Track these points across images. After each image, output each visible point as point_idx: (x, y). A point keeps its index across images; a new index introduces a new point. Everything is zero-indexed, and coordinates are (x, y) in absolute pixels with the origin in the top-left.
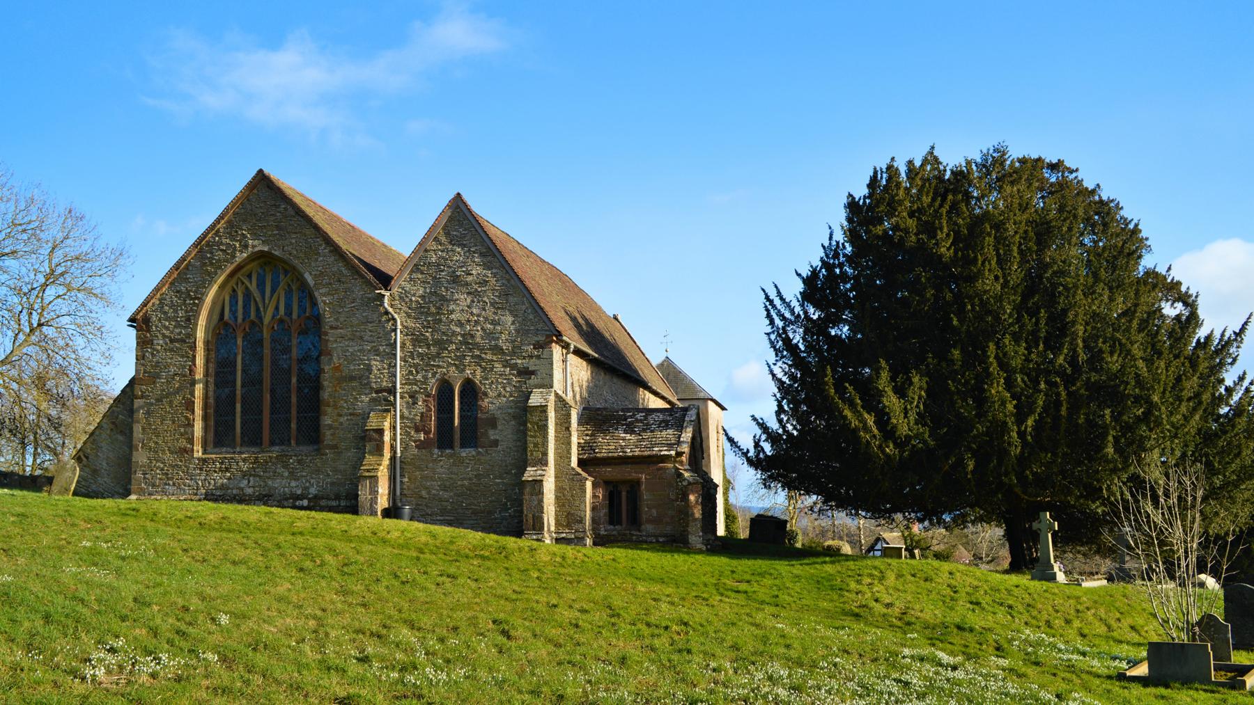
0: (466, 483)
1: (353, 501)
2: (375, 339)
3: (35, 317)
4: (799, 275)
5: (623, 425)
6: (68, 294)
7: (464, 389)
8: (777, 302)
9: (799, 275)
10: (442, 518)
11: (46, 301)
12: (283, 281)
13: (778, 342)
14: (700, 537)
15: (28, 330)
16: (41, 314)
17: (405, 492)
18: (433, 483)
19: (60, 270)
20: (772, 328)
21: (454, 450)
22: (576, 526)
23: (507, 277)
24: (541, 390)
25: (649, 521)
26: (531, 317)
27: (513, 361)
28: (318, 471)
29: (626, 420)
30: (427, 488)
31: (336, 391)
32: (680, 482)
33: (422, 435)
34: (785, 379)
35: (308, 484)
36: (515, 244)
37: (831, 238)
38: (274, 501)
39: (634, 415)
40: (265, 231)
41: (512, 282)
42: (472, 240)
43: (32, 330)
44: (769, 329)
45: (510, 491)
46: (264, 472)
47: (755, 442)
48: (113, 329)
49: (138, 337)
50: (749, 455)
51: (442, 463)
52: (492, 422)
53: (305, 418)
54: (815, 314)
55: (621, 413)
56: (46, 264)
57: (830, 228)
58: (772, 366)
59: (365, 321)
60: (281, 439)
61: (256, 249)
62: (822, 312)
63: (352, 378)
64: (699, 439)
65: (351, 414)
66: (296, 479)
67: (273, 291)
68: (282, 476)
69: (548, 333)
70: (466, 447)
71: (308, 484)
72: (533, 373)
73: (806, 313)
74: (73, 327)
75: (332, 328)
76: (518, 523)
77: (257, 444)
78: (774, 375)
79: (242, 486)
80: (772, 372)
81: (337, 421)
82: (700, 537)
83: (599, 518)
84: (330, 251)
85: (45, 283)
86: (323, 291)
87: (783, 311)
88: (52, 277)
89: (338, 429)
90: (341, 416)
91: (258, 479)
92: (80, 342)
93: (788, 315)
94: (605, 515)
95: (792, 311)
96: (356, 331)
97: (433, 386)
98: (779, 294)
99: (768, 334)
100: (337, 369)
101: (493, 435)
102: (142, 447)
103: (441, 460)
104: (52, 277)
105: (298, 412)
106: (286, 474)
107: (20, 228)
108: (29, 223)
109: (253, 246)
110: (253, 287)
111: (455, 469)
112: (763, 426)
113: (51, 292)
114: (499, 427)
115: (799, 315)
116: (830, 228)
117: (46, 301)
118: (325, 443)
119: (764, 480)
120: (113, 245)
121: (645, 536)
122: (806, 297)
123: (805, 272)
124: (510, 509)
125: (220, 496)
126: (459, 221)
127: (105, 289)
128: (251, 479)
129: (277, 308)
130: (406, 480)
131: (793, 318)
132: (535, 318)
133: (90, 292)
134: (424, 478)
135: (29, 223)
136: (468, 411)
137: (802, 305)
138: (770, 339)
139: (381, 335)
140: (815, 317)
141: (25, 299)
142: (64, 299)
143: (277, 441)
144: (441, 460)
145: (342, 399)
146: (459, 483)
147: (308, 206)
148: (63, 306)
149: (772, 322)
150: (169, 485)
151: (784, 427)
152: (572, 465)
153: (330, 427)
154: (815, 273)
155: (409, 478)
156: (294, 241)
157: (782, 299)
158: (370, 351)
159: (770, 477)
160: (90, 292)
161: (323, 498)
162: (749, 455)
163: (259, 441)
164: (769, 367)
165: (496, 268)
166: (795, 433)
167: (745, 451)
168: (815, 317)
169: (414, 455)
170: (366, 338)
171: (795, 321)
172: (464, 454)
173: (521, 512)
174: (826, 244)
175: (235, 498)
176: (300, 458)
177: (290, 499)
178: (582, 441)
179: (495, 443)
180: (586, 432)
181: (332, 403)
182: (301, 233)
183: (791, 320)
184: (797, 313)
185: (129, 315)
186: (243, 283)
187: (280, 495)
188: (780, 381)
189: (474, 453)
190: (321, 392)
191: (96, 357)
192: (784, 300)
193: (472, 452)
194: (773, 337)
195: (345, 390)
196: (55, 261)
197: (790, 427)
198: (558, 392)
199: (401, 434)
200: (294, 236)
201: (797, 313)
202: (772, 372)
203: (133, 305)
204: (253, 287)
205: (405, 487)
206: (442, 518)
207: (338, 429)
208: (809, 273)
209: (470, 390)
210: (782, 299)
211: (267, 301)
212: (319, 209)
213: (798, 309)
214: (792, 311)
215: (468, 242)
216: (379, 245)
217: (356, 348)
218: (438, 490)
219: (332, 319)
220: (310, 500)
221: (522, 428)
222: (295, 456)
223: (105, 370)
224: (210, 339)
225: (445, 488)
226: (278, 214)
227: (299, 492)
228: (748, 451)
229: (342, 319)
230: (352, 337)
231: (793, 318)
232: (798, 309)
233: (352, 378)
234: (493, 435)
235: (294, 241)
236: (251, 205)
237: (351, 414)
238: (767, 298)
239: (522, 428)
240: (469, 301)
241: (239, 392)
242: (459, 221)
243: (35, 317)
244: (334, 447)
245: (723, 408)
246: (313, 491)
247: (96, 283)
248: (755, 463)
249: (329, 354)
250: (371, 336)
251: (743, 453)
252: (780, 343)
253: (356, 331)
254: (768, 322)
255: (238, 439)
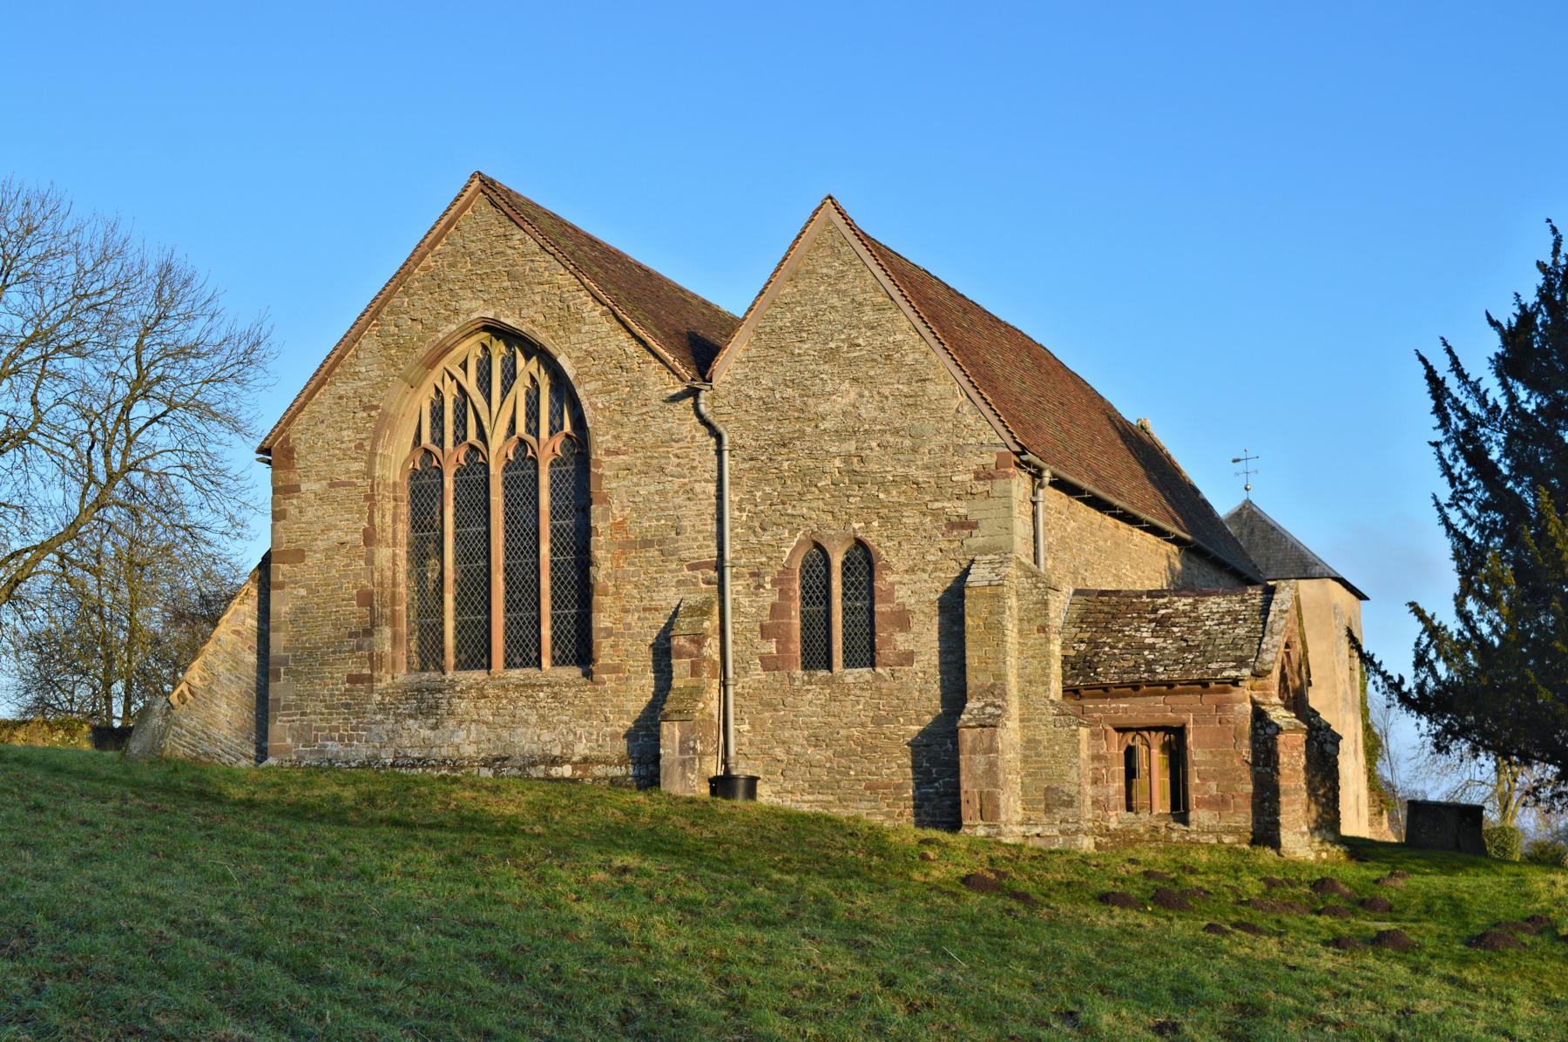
0: (855, 732)
1: (651, 768)
2: (686, 472)
3: (117, 458)
4: (1495, 324)
5: (1151, 621)
6: (170, 414)
7: (848, 559)
8: (1452, 382)
9: (1495, 324)
10: (811, 798)
11: (133, 430)
12: (526, 367)
13: (1456, 460)
14: (1303, 834)
15: (102, 478)
16: (124, 455)
17: (745, 749)
18: (795, 733)
19: (154, 373)
20: (1447, 432)
21: (831, 671)
22: (1061, 813)
23: (924, 347)
24: (991, 557)
25: (1201, 803)
26: (970, 420)
27: (937, 505)
28: (588, 714)
29: (1155, 611)
30: (784, 743)
31: (618, 566)
32: (1262, 727)
33: (774, 645)
34: (1471, 533)
35: (571, 737)
36: (942, 290)
37: (1556, 251)
38: (512, 767)
39: (1171, 602)
40: (487, 282)
41: (933, 356)
42: (857, 282)
43: (111, 477)
44: (1439, 436)
45: (936, 748)
46: (493, 715)
47: (1417, 654)
48: (245, 475)
49: (274, 481)
50: (1405, 688)
51: (810, 696)
52: (902, 620)
53: (566, 617)
54: (1530, 401)
55: (1145, 599)
56: (132, 363)
57: (1554, 230)
58: (1446, 510)
59: (667, 437)
60: (524, 652)
61: (475, 316)
62: (1546, 396)
63: (646, 544)
64: (1299, 647)
65: (645, 609)
66: (552, 727)
67: (506, 389)
68: (526, 722)
69: (1001, 449)
70: (854, 666)
71: (571, 737)
72: (973, 526)
73: (1512, 398)
74: (179, 471)
75: (608, 452)
76: (951, 806)
77: (482, 667)
78: (1450, 527)
79: (457, 740)
80: (1445, 520)
81: (620, 620)
82: (1303, 834)
83: (1107, 799)
84: (603, 314)
85: (131, 395)
86: (591, 386)
87: (1463, 399)
88: (141, 388)
89: (623, 635)
90: (627, 611)
91: (485, 728)
92: (188, 493)
93: (1473, 408)
94: (1118, 792)
95: (1483, 401)
96: (652, 457)
97: (791, 549)
98: (1455, 362)
99: (1437, 444)
100: (619, 526)
101: (902, 641)
102: (285, 674)
103: (808, 691)
104: (141, 388)
105: (553, 608)
106: (534, 719)
107: (86, 302)
108: (101, 293)
109: (469, 312)
110: (471, 385)
111: (835, 707)
112: (1434, 630)
113: (141, 411)
114: (915, 629)
115: (1496, 407)
116: (1554, 230)
117: (133, 430)
118: (600, 661)
119: (1436, 736)
120: (242, 327)
121: (1198, 833)
122: (1506, 367)
123: (1507, 315)
124: (936, 780)
125: (419, 760)
126: (832, 247)
127: (232, 405)
128: (473, 727)
129: (513, 421)
130: (746, 727)
131: (1483, 415)
132: (977, 421)
133: (205, 411)
134: (782, 724)
135: (101, 293)
136: (856, 599)
137: (1504, 384)
138: (1441, 457)
139: (695, 464)
140: (1531, 407)
141: (97, 424)
142: (163, 423)
143: (518, 660)
144: (808, 691)
145: (630, 582)
146: (842, 732)
147: (563, 235)
148: (162, 437)
149: (1445, 421)
150: (332, 739)
151: (1472, 629)
152: (1052, 697)
153: (609, 632)
154: (1526, 317)
155: (752, 725)
156: (538, 298)
157: (1461, 375)
158: (677, 492)
159: (1448, 729)
160: (205, 411)
161: (599, 763)
162: (1405, 688)
163: (484, 661)
164: (1440, 510)
165: (902, 332)
166: (1497, 642)
167: (1396, 679)
168: (1531, 407)
169: (759, 681)
170: (670, 469)
171: (1488, 418)
172: (849, 679)
173: (957, 787)
174: (1549, 262)
175: (444, 762)
176: (556, 689)
177: (542, 763)
178: (1072, 653)
179: (908, 658)
180: (1080, 635)
181: (612, 589)
182: (549, 283)
183: (1478, 417)
184: (1491, 403)
185: (257, 444)
186: (452, 377)
187: (523, 757)
188: (1461, 537)
189: (868, 677)
190: (592, 570)
191: (221, 524)
192: (1466, 377)
193: (865, 673)
194: (1447, 450)
195: (633, 564)
196: (147, 357)
197: (1485, 629)
198: (1024, 559)
199: (734, 642)
200: (538, 289)
201: (1491, 403)
202: (1445, 520)
203: (265, 425)
204: (471, 385)
205: (745, 740)
206: (811, 798)
207: (623, 635)
208: (1514, 321)
209: (863, 560)
210: (1461, 375)
211: (495, 409)
212: (584, 240)
213: (1496, 394)
214: (1483, 401)
215: (850, 286)
216: (694, 302)
217: (653, 488)
218: (802, 746)
219: (609, 437)
220: (575, 765)
221: (956, 629)
222: (549, 685)
223: (224, 541)
224: (398, 479)
225: (815, 741)
226: (509, 251)
227: (557, 752)
228: (1402, 679)
229: (625, 437)
230: (645, 469)
231: (1483, 415)
232: (1496, 394)
233: (646, 544)
234: (902, 641)
235: (538, 298)
236: (462, 236)
237: (645, 609)
238: (1431, 375)
239: (956, 629)
240: (853, 395)
241: (450, 575)
242: (832, 247)
243: (117, 458)
244: (615, 669)
245: (1361, 596)
246: (581, 749)
247: (212, 395)
248: (1418, 703)
249: (605, 500)
250: (678, 465)
251: (1390, 686)
252: (1462, 463)
253: (652, 457)
254: (1437, 422)
255: (450, 659)
